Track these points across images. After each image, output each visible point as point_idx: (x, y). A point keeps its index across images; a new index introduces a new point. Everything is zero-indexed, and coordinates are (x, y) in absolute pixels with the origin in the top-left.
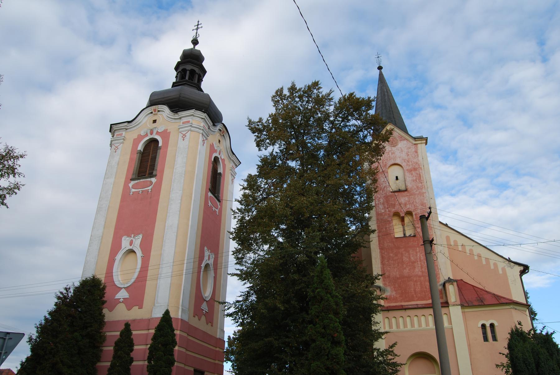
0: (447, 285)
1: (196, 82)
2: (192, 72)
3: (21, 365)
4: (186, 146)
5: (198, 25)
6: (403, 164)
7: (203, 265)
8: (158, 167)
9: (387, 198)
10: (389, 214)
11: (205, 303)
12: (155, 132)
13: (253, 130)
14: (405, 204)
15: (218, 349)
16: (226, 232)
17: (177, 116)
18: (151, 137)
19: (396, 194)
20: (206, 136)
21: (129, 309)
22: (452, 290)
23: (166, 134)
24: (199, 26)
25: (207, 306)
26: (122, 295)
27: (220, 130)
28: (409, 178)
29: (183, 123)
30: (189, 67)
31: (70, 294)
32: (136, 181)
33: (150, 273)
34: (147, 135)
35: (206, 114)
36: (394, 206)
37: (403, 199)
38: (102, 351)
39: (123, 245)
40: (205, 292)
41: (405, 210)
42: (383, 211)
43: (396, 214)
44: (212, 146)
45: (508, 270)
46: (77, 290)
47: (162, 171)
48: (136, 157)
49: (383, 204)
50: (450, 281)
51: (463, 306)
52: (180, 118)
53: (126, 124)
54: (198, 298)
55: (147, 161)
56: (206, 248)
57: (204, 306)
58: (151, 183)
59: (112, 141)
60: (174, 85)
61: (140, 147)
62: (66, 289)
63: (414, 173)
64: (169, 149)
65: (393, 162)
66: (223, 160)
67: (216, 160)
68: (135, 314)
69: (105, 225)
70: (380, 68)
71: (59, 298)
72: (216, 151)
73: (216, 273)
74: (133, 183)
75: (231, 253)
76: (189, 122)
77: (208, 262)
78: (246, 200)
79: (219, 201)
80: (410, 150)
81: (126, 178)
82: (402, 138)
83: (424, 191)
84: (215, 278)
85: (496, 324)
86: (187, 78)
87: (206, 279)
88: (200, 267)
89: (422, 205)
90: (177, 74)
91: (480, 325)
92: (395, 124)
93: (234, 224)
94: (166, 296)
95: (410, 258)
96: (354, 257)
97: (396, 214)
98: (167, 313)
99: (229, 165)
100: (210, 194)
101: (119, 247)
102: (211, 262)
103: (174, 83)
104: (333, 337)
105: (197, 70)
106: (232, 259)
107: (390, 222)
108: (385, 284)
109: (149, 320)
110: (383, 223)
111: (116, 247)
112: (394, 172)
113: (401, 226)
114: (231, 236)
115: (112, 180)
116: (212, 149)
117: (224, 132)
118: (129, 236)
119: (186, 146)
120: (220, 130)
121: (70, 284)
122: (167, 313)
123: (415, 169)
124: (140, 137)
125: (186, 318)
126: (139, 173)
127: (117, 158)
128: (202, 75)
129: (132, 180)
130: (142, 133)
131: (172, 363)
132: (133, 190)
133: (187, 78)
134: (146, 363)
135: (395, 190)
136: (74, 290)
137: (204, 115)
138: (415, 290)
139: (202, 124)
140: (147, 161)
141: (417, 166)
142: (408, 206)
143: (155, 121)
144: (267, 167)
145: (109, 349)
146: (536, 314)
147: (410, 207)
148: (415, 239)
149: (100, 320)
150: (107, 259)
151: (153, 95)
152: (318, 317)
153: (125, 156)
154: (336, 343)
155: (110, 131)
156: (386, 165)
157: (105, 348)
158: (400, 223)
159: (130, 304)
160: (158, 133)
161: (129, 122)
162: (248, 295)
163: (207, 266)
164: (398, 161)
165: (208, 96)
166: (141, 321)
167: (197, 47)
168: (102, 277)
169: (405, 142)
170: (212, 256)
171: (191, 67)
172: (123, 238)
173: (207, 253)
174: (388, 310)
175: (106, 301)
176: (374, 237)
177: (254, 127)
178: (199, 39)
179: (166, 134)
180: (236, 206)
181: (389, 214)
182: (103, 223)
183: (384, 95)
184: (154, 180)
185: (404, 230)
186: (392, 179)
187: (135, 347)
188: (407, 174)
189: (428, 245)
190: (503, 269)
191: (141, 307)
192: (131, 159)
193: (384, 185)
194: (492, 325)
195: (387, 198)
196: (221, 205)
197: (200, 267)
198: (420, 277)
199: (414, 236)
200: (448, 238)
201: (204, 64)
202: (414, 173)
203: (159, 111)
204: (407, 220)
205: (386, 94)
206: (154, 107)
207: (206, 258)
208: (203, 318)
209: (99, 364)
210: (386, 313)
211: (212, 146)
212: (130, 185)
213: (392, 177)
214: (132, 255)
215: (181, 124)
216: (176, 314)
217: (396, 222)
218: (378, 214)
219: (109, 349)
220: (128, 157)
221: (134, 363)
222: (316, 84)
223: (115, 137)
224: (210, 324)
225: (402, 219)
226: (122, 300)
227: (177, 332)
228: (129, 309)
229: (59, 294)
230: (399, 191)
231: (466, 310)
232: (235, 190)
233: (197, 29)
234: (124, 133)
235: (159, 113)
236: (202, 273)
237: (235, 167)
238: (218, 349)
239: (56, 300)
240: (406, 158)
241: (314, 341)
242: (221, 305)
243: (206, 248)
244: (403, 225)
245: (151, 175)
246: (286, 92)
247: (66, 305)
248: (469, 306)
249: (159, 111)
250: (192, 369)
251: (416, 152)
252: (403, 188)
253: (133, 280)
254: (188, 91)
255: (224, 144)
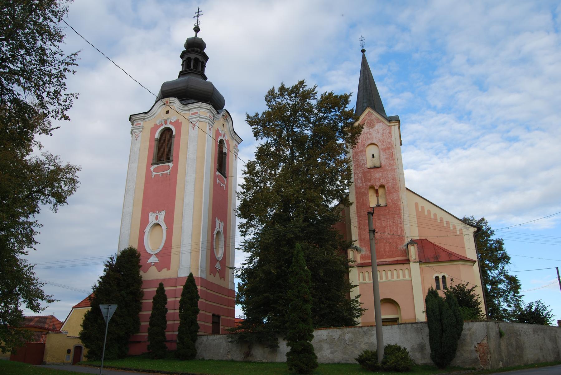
0: (409, 246)
1: (200, 70)
2: (196, 60)
3: (85, 316)
4: (195, 132)
5: (198, 12)
6: (379, 144)
7: (215, 233)
8: (174, 153)
9: (364, 173)
10: (366, 188)
11: (218, 263)
12: (168, 122)
13: (251, 123)
14: (379, 179)
15: (230, 298)
16: (232, 210)
17: (186, 108)
18: (166, 126)
19: (372, 170)
20: (212, 122)
21: (160, 270)
22: (413, 251)
23: (178, 124)
24: (200, 13)
25: (219, 265)
26: (153, 260)
27: (223, 115)
28: (383, 156)
29: (192, 114)
30: (193, 56)
31: (114, 262)
32: (156, 166)
33: (174, 244)
34: (162, 125)
35: (211, 106)
36: (370, 180)
37: (377, 174)
38: (141, 303)
39: (150, 220)
40: (218, 254)
41: (378, 184)
42: (361, 185)
43: (372, 187)
44: (217, 132)
45: (465, 232)
46: (119, 258)
47: (178, 157)
48: (155, 144)
49: (361, 179)
50: (412, 242)
51: (420, 262)
52: (189, 110)
53: (143, 115)
54: (213, 259)
55: (164, 148)
56: (216, 219)
57: (218, 266)
58: (169, 167)
59: (132, 130)
60: (181, 74)
61: (157, 135)
62: (111, 258)
63: (387, 152)
64: (182, 137)
65: (370, 142)
66: (227, 141)
67: (221, 142)
68: (164, 274)
69: (134, 203)
70: (363, 51)
71: (107, 266)
72: (221, 135)
73: (225, 237)
74: (154, 167)
75: (237, 227)
76: (197, 113)
77: (219, 230)
78: (248, 185)
79: (226, 177)
80: (385, 131)
81: (148, 163)
82: (379, 121)
83: (395, 167)
84: (225, 241)
85: (447, 276)
86: (192, 67)
87: (218, 248)
88: (213, 235)
89: (393, 179)
90: (183, 62)
91: (434, 277)
92: (374, 108)
93: (238, 203)
94: (187, 262)
95: (381, 224)
96: (333, 228)
97: (372, 187)
98: (191, 275)
99: (232, 144)
100: (218, 173)
101: (148, 221)
102: (221, 229)
103: (181, 72)
104: (304, 298)
105: (200, 58)
106: (238, 233)
107: (366, 194)
108: (361, 245)
109: (176, 279)
110: (361, 196)
111: (144, 221)
112: (371, 150)
113: (376, 198)
114: (237, 214)
115: (135, 165)
116: (218, 133)
117: (226, 116)
118: (155, 212)
119: (195, 132)
120: (223, 115)
121: (114, 254)
122: (191, 275)
123: (389, 148)
124: (156, 127)
125: (204, 276)
126: (158, 159)
127: (138, 146)
128: (204, 61)
129: (153, 164)
130: (158, 123)
131: (197, 312)
132: (155, 173)
133: (192, 67)
134: (178, 311)
135: (372, 166)
136: (117, 259)
137: (209, 106)
138: (384, 250)
139: (208, 114)
140: (164, 148)
141: (390, 146)
142: (382, 181)
143: (168, 112)
144: (262, 153)
145: (148, 301)
146: (510, 258)
147: (382, 182)
148: (386, 208)
149: (138, 281)
150: (138, 231)
151: (164, 85)
152: (295, 285)
153: (144, 146)
154: (306, 301)
155: (130, 120)
156: (364, 145)
157: (144, 301)
158: (375, 195)
159: (160, 266)
160: (171, 123)
161: (145, 113)
162: (251, 259)
163: (218, 233)
164: (375, 141)
165: (211, 84)
166: (170, 280)
167: (200, 35)
168: (135, 246)
169: (381, 124)
170: (222, 224)
171: (194, 55)
172: (150, 214)
173: (218, 222)
174: (363, 267)
175: (141, 266)
176: (353, 209)
177: (252, 121)
178: (200, 27)
179: (178, 124)
180: (240, 189)
181: (366, 188)
182: (132, 201)
183: (366, 78)
184: (171, 164)
185: (378, 200)
186: (369, 156)
187: (168, 300)
188: (382, 152)
189: (372, 234)
190: (461, 230)
191: (169, 269)
192: (150, 146)
193: (363, 162)
194: (444, 277)
195: (364, 173)
196: (227, 181)
197: (213, 235)
198: (389, 239)
199: (386, 206)
200: (416, 204)
201: (206, 51)
202: (387, 152)
203: (170, 103)
204: (381, 191)
205: (367, 77)
206: (166, 99)
207: (217, 227)
208: (217, 274)
209: (141, 313)
210: (361, 268)
211: (217, 132)
212: (152, 169)
213: (370, 155)
214: (158, 227)
215: (191, 115)
216: (198, 274)
217: (371, 193)
218: (357, 188)
219: (148, 301)
220: (148, 144)
221: (169, 312)
222: (302, 83)
223: (135, 126)
224: (223, 279)
225: (377, 192)
226: (153, 264)
227: (199, 288)
228: (160, 270)
229: (107, 263)
230: (375, 167)
231: (424, 266)
232: (239, 177)
233: (198, 16)
234: (142, 122)
235: (171, 104)
236: (214, 243)
237: (237, 144)
238: (230, 298)
239: (105, 267)
240: (381, 138)
241: (292, 300)
242: (230, 270)
243: (216, 219)
244: (377, 196)
245: (168, 160)
246: (277, 91)
247: (113, 271)
248: (426, 263)
249: (170, 103)
250: (211, 314)
251: (390, 133)
252: (378, 165)
253: (160, 249)
254: (194, 80)
255: (228, 126)
